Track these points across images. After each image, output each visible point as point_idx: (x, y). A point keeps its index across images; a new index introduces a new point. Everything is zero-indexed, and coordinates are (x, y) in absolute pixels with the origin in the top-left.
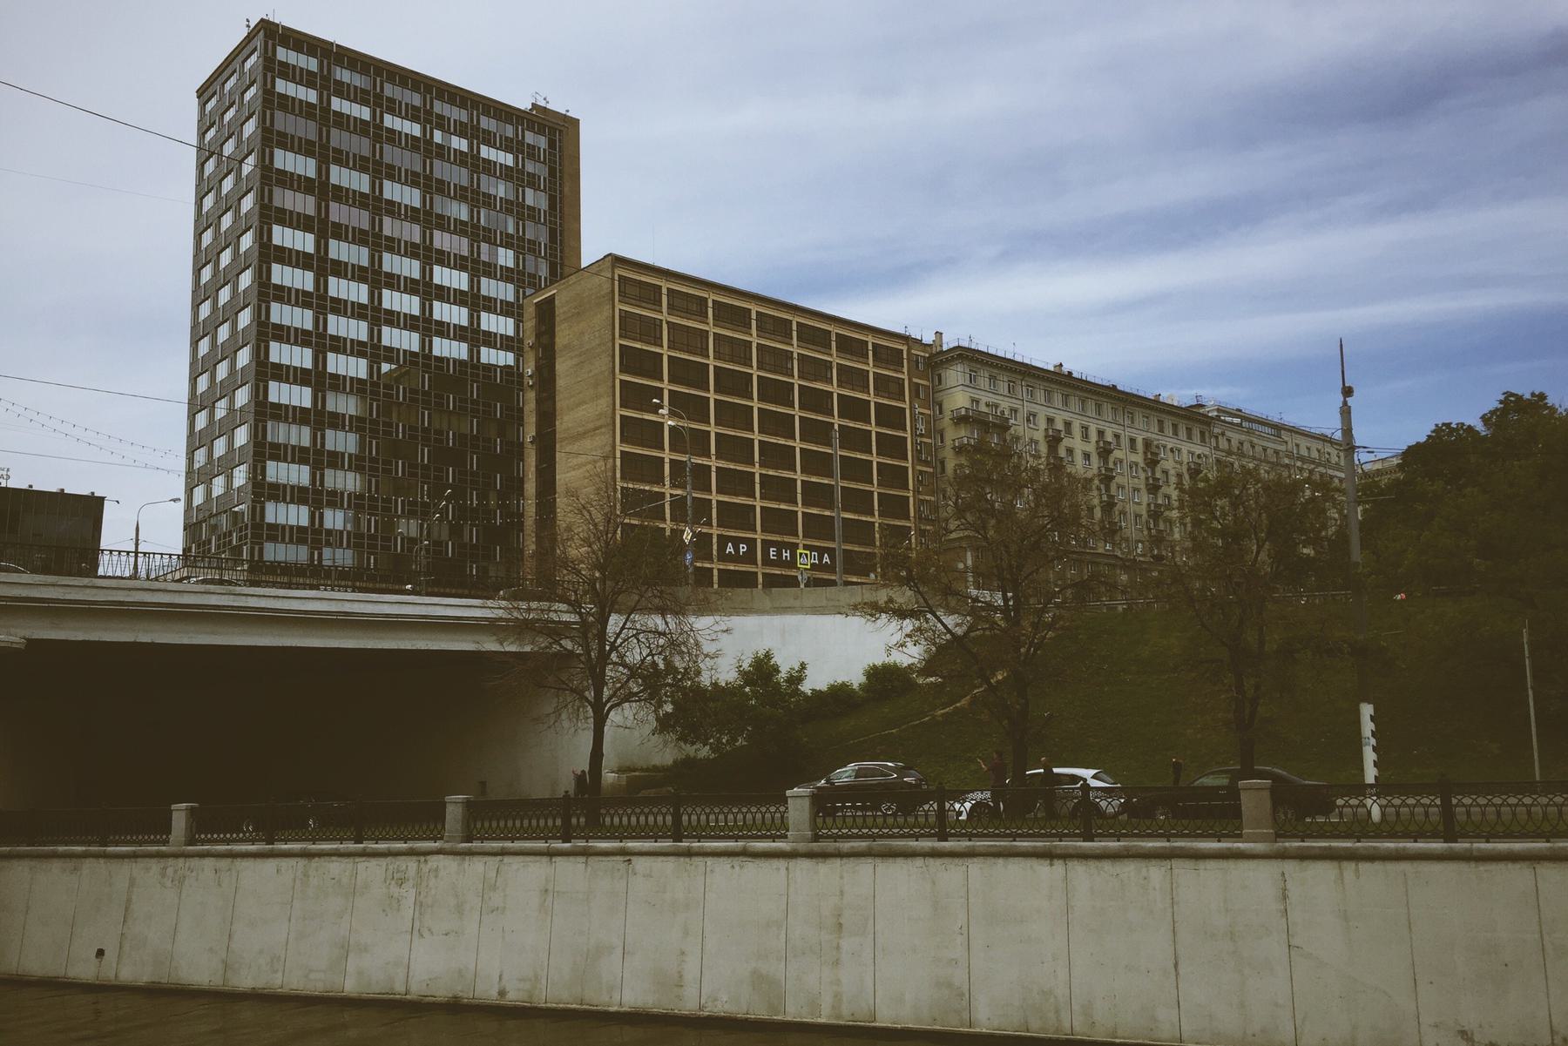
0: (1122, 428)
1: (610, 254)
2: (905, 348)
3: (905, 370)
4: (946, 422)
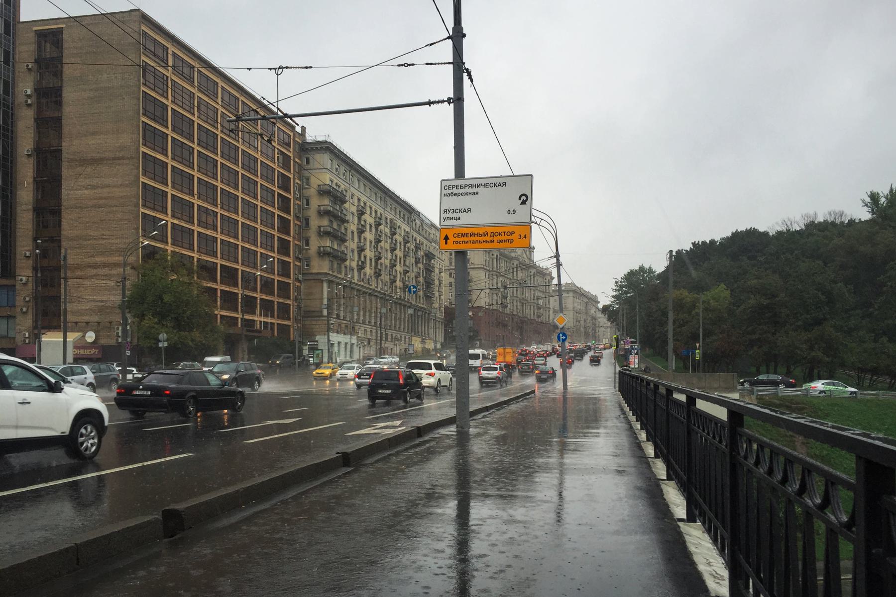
0: (348, 185)
1: (138, 10)
2: (292, 134)
3: (291, 150)
4: (312, 192)
